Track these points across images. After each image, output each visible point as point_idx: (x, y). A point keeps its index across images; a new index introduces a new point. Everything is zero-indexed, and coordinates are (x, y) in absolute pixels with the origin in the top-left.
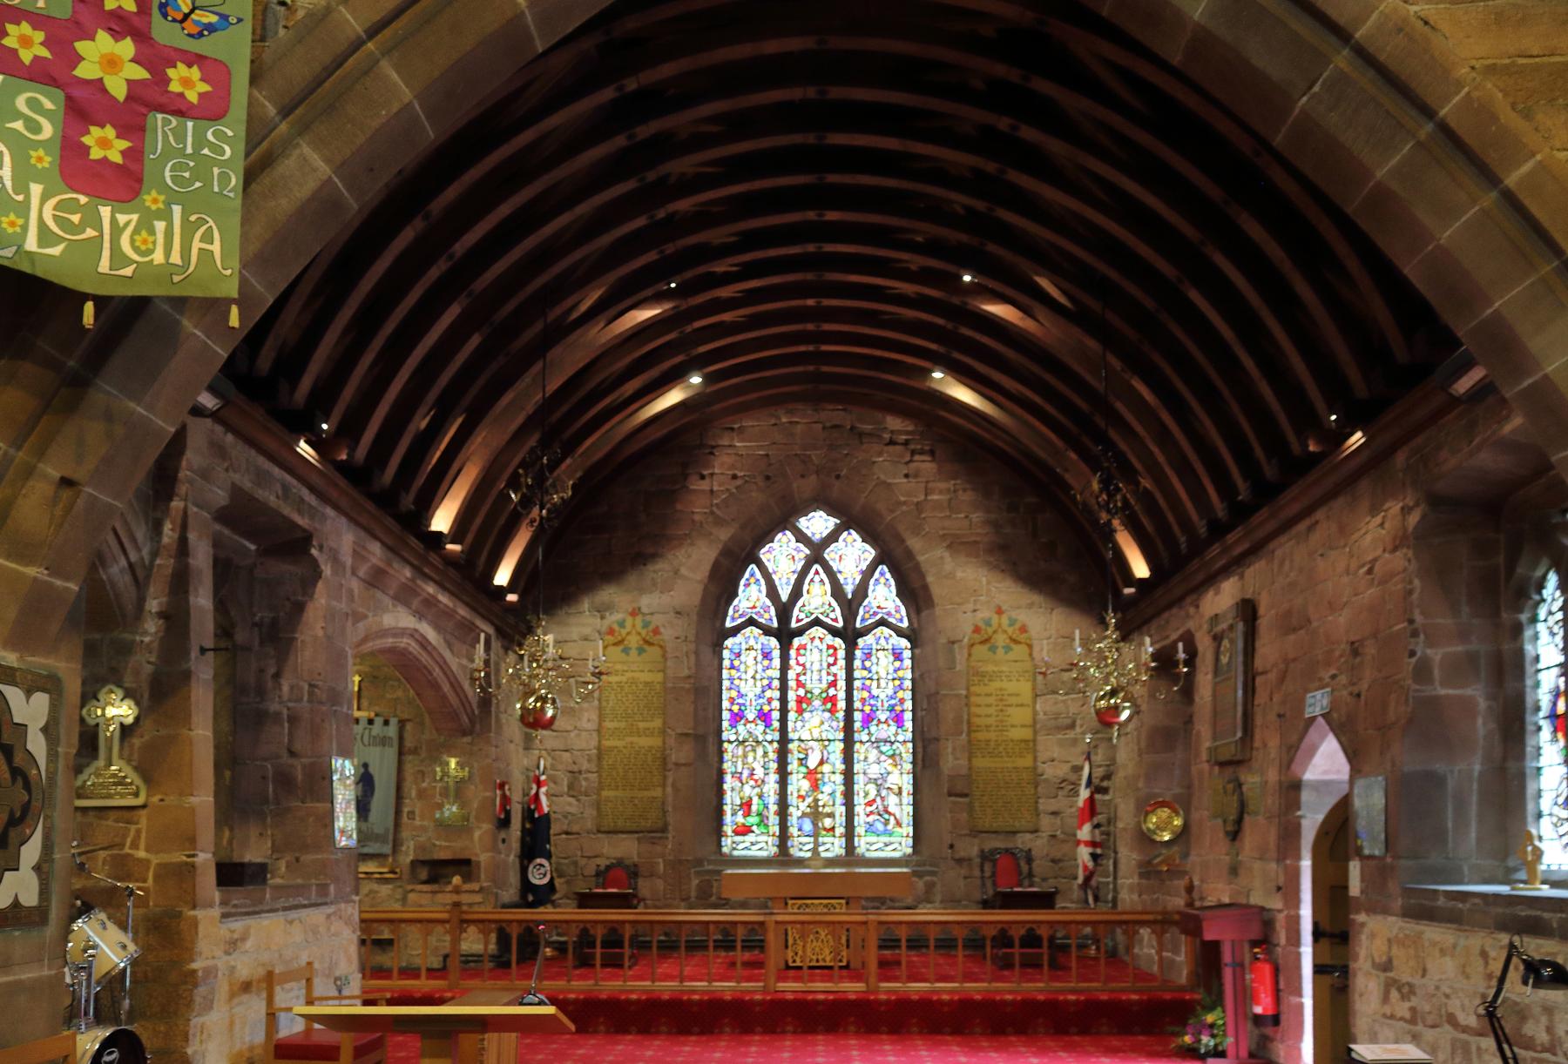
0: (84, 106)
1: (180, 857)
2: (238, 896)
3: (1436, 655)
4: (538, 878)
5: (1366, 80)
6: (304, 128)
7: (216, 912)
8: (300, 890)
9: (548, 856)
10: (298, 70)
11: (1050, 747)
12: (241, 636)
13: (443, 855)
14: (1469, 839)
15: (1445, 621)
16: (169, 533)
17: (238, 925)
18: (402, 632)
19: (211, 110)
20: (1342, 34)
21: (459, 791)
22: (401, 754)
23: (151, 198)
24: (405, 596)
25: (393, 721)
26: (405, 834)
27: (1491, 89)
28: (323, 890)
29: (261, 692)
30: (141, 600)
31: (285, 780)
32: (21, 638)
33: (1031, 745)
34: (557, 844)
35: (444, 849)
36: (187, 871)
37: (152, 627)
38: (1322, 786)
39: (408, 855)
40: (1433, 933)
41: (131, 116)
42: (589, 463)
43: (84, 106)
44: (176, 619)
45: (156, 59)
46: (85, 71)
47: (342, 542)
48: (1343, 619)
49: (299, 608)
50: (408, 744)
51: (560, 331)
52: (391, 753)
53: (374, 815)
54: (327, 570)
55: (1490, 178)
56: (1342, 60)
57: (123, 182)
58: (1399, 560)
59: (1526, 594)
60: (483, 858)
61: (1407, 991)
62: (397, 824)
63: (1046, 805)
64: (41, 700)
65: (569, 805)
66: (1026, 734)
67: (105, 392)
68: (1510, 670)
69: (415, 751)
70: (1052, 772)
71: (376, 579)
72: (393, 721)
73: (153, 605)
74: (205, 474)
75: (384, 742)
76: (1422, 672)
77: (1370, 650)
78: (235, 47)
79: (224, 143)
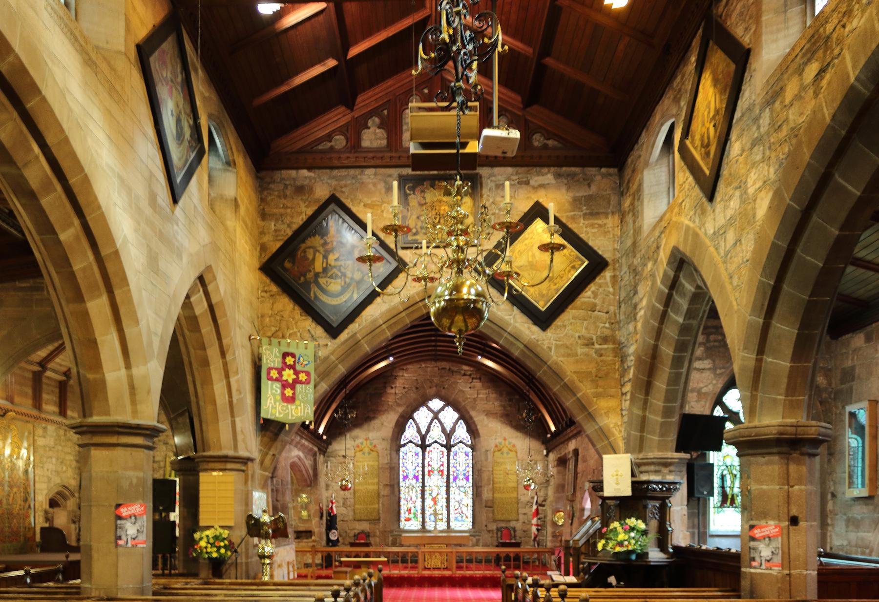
5: (512, 339)
9: (336, 529)
10: (322, 369)
19: (307, 382)
21: (306, 507)
23: (297, 402)
34: (339, 525)
35: (302, 527)
41: (293, 386)
45: (297, 373)
46: (284, 378)
57: (292, 400)
63: (521, 511)
65: (343, 510)
66: (514, 485)
78: (311, 368)
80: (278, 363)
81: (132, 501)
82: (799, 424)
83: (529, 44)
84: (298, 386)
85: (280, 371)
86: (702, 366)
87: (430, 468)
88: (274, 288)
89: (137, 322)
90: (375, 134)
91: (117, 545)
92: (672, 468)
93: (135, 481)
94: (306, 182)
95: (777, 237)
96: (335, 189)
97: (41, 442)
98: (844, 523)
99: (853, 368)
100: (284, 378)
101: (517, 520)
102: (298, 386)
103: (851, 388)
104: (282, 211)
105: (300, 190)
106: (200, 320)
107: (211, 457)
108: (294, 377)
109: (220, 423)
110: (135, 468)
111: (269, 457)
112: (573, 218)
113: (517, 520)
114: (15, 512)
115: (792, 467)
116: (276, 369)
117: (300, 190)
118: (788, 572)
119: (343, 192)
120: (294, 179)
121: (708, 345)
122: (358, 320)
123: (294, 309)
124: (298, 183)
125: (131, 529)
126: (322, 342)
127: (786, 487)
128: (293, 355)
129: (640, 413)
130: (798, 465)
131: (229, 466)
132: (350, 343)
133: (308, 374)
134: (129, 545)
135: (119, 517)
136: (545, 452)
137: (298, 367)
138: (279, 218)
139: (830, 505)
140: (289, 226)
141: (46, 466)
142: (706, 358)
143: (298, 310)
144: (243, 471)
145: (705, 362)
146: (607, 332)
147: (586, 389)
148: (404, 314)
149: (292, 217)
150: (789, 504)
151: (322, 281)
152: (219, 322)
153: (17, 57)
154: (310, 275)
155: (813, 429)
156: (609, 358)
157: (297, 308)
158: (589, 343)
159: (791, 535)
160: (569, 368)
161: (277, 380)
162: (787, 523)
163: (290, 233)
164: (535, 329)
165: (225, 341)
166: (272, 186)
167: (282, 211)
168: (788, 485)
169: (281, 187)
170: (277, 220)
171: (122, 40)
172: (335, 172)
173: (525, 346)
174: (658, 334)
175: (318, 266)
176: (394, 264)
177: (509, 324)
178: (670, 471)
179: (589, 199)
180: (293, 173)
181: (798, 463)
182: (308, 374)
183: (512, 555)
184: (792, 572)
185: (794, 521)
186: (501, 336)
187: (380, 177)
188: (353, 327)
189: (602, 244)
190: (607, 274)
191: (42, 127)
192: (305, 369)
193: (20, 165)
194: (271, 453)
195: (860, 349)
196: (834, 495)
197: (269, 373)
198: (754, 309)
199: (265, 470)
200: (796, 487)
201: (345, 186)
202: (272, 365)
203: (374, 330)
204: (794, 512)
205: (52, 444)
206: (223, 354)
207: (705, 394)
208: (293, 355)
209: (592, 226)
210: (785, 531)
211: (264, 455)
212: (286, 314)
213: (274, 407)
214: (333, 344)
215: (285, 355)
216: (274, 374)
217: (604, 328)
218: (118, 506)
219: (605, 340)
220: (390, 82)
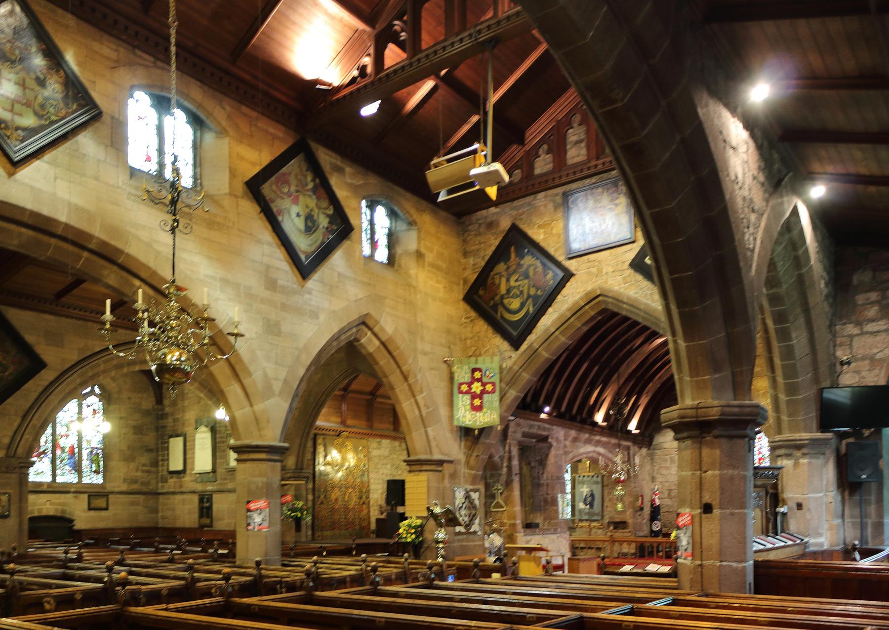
0: (474, 396)
1: (513, 522)
2: (528, 531)
4: (655, 529)
6: (510, 387)
7: (522, 534)
8: (548, 530)
9: (659, 520)
10: (508, 378)
12: (533, 464)
13: (618, 520)
16: (507, 448)
17: (529, 538)
18: (589, 452)
19: (493, 391)
21: (621, 499)
22: (603, 486)
23: (485, 410)
24: (588, 442)
26: (605, 513)
28: (556, 530)
29: (539, 478)
30: (502, 464)
31: (546, 501)
32: (473, 483)
34: (662, 516)
35: (618, 519)
36: (514, 525)
37: (505, 470)
39: (606, 521)
41: (480, 396)
42: (662, 381)
43: (474, 396)
44: (509, 468)
45: (484, 385)
46: (473, 390)
47: (560, 434)
49: (547, 455)
50: (605, 483)
51: (631, 352)
52: (600, 486)
54: (554, 444)
57: (479, 408)
60: (630, 521)
64: (477, 494)
65: (667, 502)
67: (482, 439)
69: (607, 485)
71: (575, 440)
73: (505, 464)
74: (515, 432)
75: (597, 483)
78: (496, 379)
79: (496, 397)
80: (467, 378)
81: (257, 498)
82: (700, 406)
85: (470, 384)
86: (876, 329)
87: (760, 456)
88: (473, 314)
89: (250, 375)
90: (545, 160)
91: (247, 530)
92: (805, 451)
93: (260, 485)
94: (494, 218)
96: (515, 219)
97: (375, 453)
100: (473, 390)
104: (477, 247)
105: (491, 225)
106: (376, 356)
108: (482, 388)
109: (413, 434)
110: (260, 475)
111: (473, 459)
114: (351, 507)
115: (705, 451)
116: (466, 383)
117: (491, 225)
118: (699, 562)
119: (521, 219)
120: (486, 218)
121: (884, 302)
122: (534, 331)
123: (487, 330)
124: (489, 220)
125: (257, 519)
126: (507, 354)
127: (699, 472)
128: (480, 370)
130: (711, 448)
131: (425, 467)
132: (530, 353)
133: (493, 384)
134: (256, 529)
135: (249, 510)
137: (485, 380)
138: (475, 253)
140: (483, 258)
141: (381, 472)
142: (881, 319)
143: (490, 331)
144: (440, 471)
145: (880, 323)
148: (573, 319)
149: (485, 250)
150: (701, 490)
151: (506, 301)
152: (394, 354)
153: (98, 238)
154: (497, 298)
155: (715, 409)
157: (490, 328)
159: (704, 524)
161: (467, 392)
162: (699, 511)
163: (483, 264)
165: (404, 368)
166: (470, 227)
167: (477, 247)
168: (701, 470)
169: (477, 226)
170: (474, 256)
171: (227, 185)
172: (516, 203)
175: (503, 290)
176: (561, 274)
178: (804, 454)
180: (484, 212)
181: (711, 446)
182: (493, 384)
183: (647, 545)
184: (704, 562)
185: (707, 508)
187: (548, 199)
188: (531, 338)
191: (135, 270)
192: (491, 380)
193: (130, 294)
194: (475, 454)
197: (460, 388)
199: (471, 468)
200: (709, 473)
201: (523, 213)
202: (462, 381)
203: (548, 338)
204: (707, 499)
205: (386, 453)
206: (406, 378)
207: (881, 360)
210: (697, 520)
211: (468, 456)
212: (482, 334)
213: (465, 416)
214: (515, 355)
215: (474, 370)
216: (464, 388)
218: (248, 502)
220: (550, 111)
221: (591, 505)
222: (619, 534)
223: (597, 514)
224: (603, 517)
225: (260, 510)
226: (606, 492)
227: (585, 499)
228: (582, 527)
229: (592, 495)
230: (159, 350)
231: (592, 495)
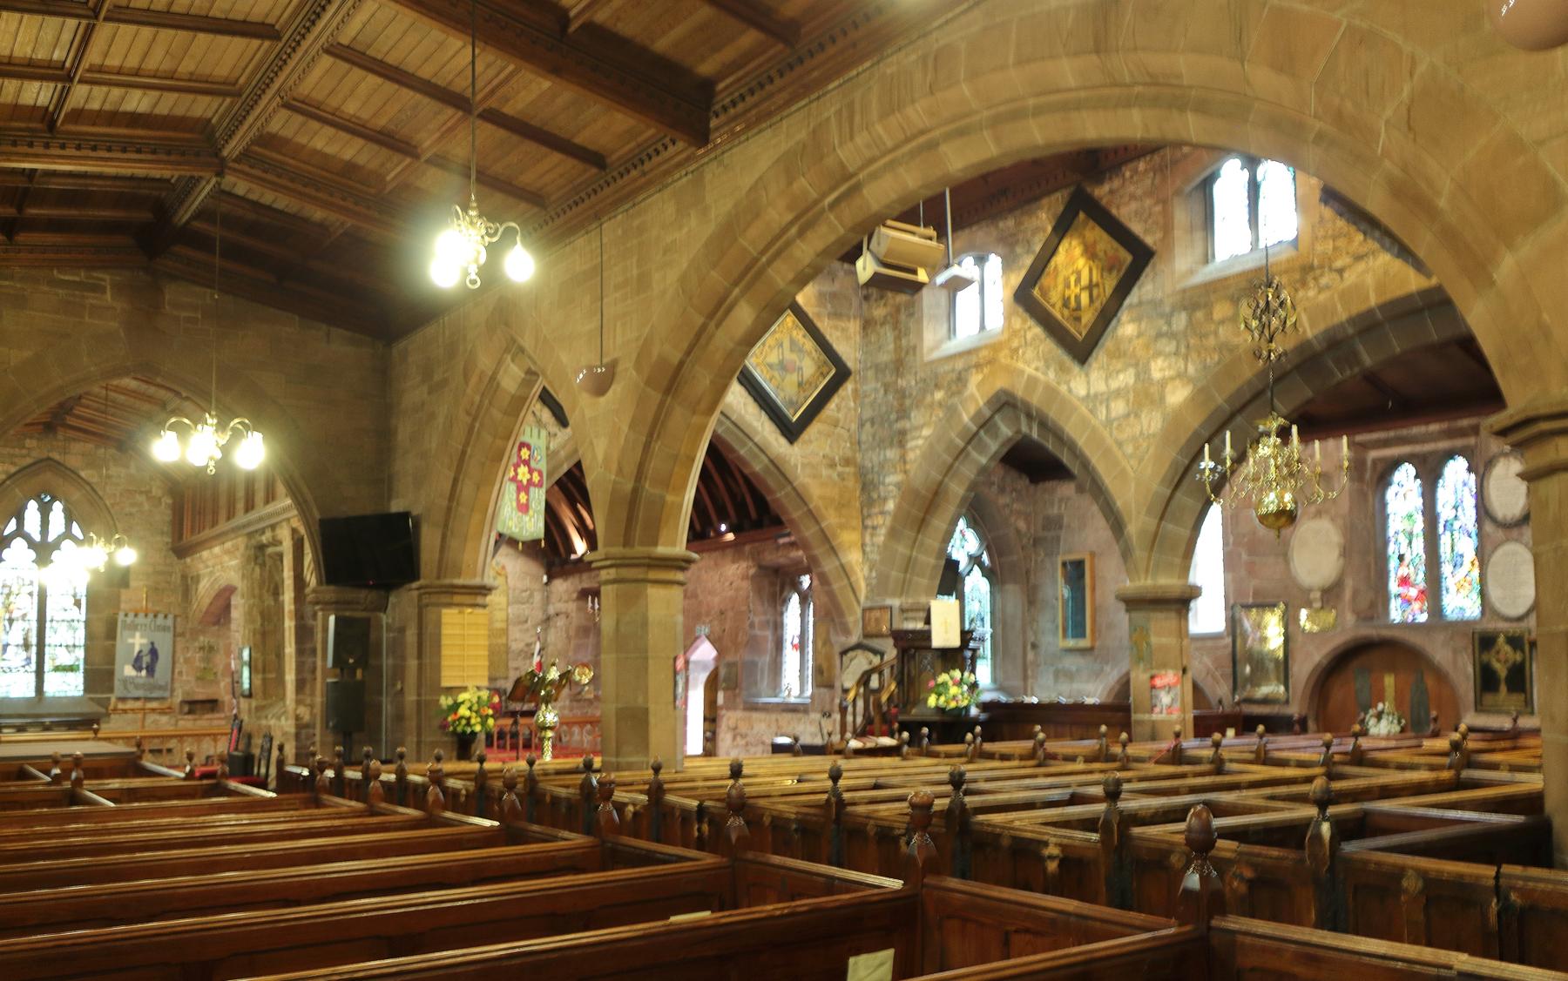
3: (757, 620)
5: (756, 450)
11: (515, 633)
13: (200, 697)
14: (764, 684)
15: (760, 608)
20: (790, 483)
25: (170, 617)
26: (177, 685)
27: (820, 503)
33: (505, 632)
35: (201, 693)
38: (702, 665)
40: (755, 715)
45: (531, 471)
48: (717, 600)
50: (179, 630)
52: (169, 636)
53: (157, 674)
55: (817, 522)
56: (789, 488)
58: (746, 585)
59: (785, 601)
61: (743, 736)
62: (172, 679)
63: (512, 664)
66: (503, 625)
68: (778, 626)
69: (183, 635)
70: (515, 646)
72: (170, 617)
75: (164, 629)
76: (752, 626)
77: (730, 614)
83: (1312, 327)
84: (532, 489)
95: (1201, 426)
98: (1051, 677)
99: (1060, 517)
101: (506, 678)
102: (532, 489)
103: (1058, 539)
107: (464, 587)
112: (819, 315)
113: (506, 678)
125: (1165, 699)
129: (907, 552)
133: (540, 474)
135: (1153, 687)
136: (545, 578)
137: (533, 464)
139: (1030, 656)
146: (849, 454)
147: (831, 519)
156: (851, 483)
158: (832, 465)
160: (816, 492)
164: (783, 441)
173: (771, 461)
174: (949, 470)
177: (757, 433)
179: (834, 296)
186: (744, 444)
189: (848, 351)
190: (849, 387)
195: (1068, 499)
196: (1034, 646)
198: (1163, 481)
208: (529, 448)
209: (836, 328)
217: (845, 448)
219: (847, 462)
221: (151, 670)
222: (204, 722)
223: (160, 688)
224: (172, 691)
225: (1169, 688)
226: (179, 647)
227: (138, 658)
228: (125, 711)
229: (154, 652)
230: (952, 412)
231: (154, 652)
